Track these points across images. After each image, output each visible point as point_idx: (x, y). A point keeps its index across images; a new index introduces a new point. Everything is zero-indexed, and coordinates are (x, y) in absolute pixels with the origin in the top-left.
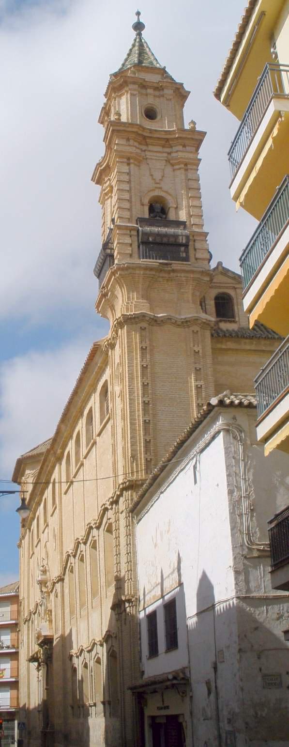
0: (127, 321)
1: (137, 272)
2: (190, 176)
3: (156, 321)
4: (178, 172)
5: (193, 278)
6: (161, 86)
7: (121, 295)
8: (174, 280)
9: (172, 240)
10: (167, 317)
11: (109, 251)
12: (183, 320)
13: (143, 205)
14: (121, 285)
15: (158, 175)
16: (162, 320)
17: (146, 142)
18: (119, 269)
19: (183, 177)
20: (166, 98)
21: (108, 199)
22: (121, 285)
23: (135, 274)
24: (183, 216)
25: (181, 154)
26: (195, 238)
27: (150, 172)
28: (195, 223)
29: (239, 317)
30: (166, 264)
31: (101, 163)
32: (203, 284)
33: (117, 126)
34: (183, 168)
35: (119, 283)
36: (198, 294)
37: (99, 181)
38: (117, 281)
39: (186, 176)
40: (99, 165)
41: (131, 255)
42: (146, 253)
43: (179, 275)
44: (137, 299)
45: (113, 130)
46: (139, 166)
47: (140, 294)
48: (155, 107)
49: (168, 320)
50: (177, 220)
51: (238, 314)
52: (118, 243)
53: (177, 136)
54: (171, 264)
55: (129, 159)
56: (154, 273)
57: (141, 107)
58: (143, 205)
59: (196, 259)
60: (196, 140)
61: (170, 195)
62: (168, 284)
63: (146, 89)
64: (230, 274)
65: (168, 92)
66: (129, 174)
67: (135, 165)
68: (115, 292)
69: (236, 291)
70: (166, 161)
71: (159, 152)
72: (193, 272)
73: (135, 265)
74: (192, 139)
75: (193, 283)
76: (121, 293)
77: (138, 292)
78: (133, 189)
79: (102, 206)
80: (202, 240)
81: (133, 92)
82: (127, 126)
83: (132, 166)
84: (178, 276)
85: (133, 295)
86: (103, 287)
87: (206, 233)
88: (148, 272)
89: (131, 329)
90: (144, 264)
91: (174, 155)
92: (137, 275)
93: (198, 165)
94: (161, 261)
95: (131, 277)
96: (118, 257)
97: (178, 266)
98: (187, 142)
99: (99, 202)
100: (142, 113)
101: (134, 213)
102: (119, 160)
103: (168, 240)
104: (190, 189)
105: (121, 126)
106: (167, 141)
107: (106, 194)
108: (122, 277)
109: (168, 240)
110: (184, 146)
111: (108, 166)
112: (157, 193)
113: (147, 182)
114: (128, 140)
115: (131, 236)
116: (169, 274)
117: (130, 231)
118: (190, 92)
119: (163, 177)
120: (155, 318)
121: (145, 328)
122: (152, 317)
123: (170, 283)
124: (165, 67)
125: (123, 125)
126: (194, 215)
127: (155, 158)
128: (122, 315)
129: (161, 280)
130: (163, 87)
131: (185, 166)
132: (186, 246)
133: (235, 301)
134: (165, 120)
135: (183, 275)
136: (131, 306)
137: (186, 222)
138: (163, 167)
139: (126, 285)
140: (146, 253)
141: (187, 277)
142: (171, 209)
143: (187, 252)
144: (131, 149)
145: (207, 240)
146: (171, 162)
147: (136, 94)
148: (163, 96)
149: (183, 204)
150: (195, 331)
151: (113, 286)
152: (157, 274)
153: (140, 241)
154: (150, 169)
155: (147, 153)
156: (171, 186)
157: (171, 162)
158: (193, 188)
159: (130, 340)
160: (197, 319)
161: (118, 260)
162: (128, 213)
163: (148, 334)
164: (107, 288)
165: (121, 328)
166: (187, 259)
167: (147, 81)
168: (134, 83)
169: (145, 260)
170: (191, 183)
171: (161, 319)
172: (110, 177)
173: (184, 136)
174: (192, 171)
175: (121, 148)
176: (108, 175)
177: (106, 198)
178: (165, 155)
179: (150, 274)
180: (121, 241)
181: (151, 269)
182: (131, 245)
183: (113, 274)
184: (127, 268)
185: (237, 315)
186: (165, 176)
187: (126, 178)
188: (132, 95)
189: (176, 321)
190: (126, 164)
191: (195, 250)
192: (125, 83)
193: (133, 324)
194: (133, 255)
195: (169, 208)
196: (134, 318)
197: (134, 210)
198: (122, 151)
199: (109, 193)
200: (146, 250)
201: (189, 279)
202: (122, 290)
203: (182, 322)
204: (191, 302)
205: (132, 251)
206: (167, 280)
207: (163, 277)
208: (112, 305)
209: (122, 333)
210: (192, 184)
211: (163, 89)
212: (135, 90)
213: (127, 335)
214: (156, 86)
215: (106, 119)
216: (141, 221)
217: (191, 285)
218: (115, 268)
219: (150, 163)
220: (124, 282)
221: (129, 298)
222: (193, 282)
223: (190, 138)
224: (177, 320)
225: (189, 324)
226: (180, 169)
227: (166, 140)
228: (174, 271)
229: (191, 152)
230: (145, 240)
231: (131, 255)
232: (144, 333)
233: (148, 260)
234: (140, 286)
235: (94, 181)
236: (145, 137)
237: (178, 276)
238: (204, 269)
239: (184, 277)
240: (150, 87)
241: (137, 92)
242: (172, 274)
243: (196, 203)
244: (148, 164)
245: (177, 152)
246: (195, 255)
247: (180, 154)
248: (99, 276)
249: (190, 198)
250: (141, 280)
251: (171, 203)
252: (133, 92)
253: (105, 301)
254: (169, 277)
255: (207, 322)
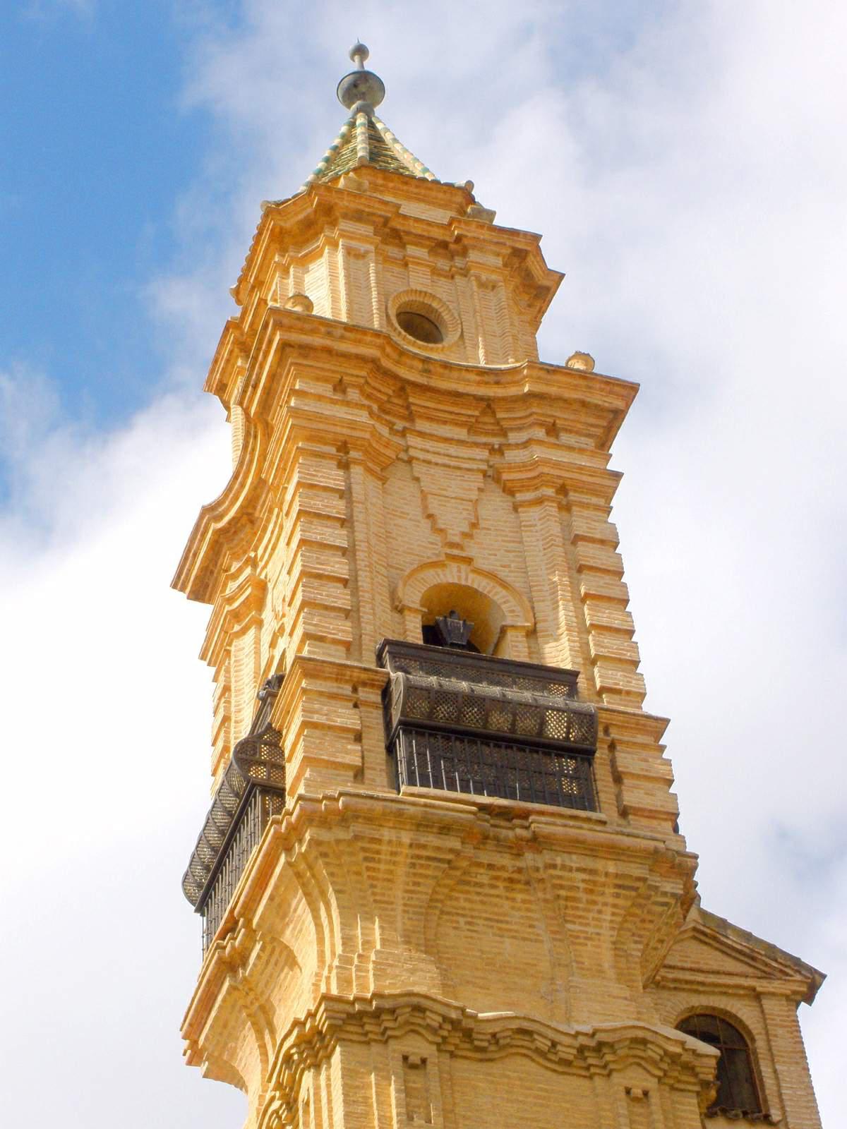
0: (354, 1024)
1: (387, 834)
2: (581, 524)
3: (468, 1034)
4: (531, 515)
5: (617, 876)
6: (458, 239)
7: (313, 935)
8: (541, 880)
9: (527, 725)
10: (515, 1025)
11: (260, 773)
12: (582, 1040)
13: (400, 610)
14: (316, 892)
15: (454, 520)
16: (494, 1035)
17: (408, 407)
18: (309, 818)
19: (556, 529)
20: (478, 278)
21: (244, 631)
22: (316, 892)
23: (379, 841)
24: (559, 654)
25: (533, 452)
26: (615, 734)
27: (425, 507)
28: (609, 683)
29: (783, 1108)
30: (505, 814)
31: (219, 503)
32: (659, 909)
33: (302, 331)
34: (549, 499)
35: (304, 885)
36: (635, 949)
37: (201, 592)
38: (299, 875)
39: (567, 527)
40: (211, 512)
41: (359, 774)
42: (423, 765)
43: (559, 861)
44: (383, 945)
45: (284, 345)
46: (384, 480)
47: (399, 925)
48: (435, 305)
49: (519, 1039)
50: (535, 662)
51: (780, 1095)
52: (305, 724)
53: (526, 389)
54: (525, 815)
55: (344, 447)
56: (454, 843)
57: (384, 297)
58: (400, 610)
59: (624, 812)
60: (598, 410)
61: (504, 584)
62: (513, 900)
63: (403, 246)
64: (732, 940)
65: (487, 261)
66: (345, 494)
67: (369, 471)
68: (283, 932)
69: (761, 1006)
70: (485, 475)
71: (461, 442)
72: (615, 852)
73: (378, 806)
74: (584, 404)
75: (620, 902)
76: (312, 928)
77: (388, 923)
78: (362, 546)
79: (213, 670)
80: (644, 746)
81: (354, 244)
82: (339, 332)
83: (357, 471)
84: (554, 866)
85: (367, 932)
86: (231, 928)
87: (657, 719)
88: (431, 839)
89: (363, 1064)
90: (414, 804)
91: (513, 456)
92: (384, 848)
93: (608, 494)
94: (485, 799)
95: (362, 855)
96: (307, 774)
97: (554, 824)
98: (562, 416)
99: (203, 657)
100: (388, 316)
101: (368, 628)
102: (304, 462)
103: (513, 724)
104: (580, 569)
105: (313, 331)
106: (487, 411)
107: (236, 616)
108: (325, 855)
109: (513, 724)
110: (553, 430)
111: (260, 483)
112: (453, 575)
113: (416, 540)
114: (340, 387)
115: (356, 706)
116: (519, 855)
117: (355, 690)
118: (563, 276)
119: (474, 525)
120: (467, 1023)
121: (424, 1061)
122: (454, 1015)
123: (519, 896)
124: (470, 184)
125: (323, 329)
126: (605, 658)
127: (446, 461)
128: (326, 998)
129: (485, 879)
130: (465, 241)
131: (558, 492)
132: (584, 754)
133: (760, 1044)
134: (476, 346)
135: (575, 861)
136: (359, 969)
137: (575, 674)
138: (474, 495)
139: (337, 892)
140: (423, 765)
141: (592, 872)
142: (510, 635)
143: (585, 780)
144: (353, 416)
145: (662, 748)
146: (505, 476)
147: (367, 252)
148: (465, 272)
149: (557, 618)
150: (637, 1092)
151: (280, 908)
152: (469, 851)
153: (396, 717)
154: (424, 496)
155: (413, 440)
156: (508, 559)
157: (505, 476)
158: (598, 573)
159: (360, 1109)
160: (644, 1042)
161: (307, 786)
162: (347, 626)
163: (435, 1087)
164: (248, 922)
165: (317, 1066)
166: (587, 800)
167: (405, 217)
168: (359, 216)
169: (418, 789)
170: (588, 553)
171: (491, 1029)
172: (256, 550)
173: (553, 390)
174: (586, 513)
175: (310, 406)
176: (249, 543)
177: (237, 628)
178: (484, 454)
179: (438, 849)
180: (315, 718)
181: (445, 829)
182: (358, 738)
183: (284, 843)
184: (345, 818)
185: (773, 1100)
186: (483, 524)
187: (337, 507)
188: (349, 252)
189: (554, 1044)
190: (334, 463)
191: (618, 779)
192: (327, 213)
193: (368, 1043)
194: (368, 774)
195: (503, 630)
196: (377, 1014)
197: (366, 617)
198: (319, 417)
199: (250, 610)
200: (421, 755)
201: (603, 879)
202: (316, 918)
203: (582, 1049)
204: (611, 973)
205: (363, 758)
206: (511, 880)
207: (491, 866)
208: (262, 1008)
209: (317, 1088)
210: (588, 553)
211: (464, 252)
212: (364, 239)
213: (345, 1086)
214: (441, 238)
215: (276, 259)
216: (397, 650)
217: (609, 910)
218: (293, 818)
219: (423, 478)
220: (332, 874)
221: (347, 941)
222: (617, 896)
223: (576, 400)
224: (558, 1038)
225: (608, 1057)
226: (539, 501)
227: (484, 404)
228: (537, 842)
229: (581, 451)
230: (417, 717)
231: (359, 774)
232: (417, 1080)
233: (432, 791)
234: (398, 893)
235: (183, 589)
236: (404, 387)
237: (554, 866)
238: (661, 845)
239: (579, 870)
240: (420, 240)
241: (372, 248)
242: (529, 856)
243: (608, 616)
244: (417, 479)
245: (526, 444)
246: (619, 797)
247: (538, 453)
248: (202, 905)
249: (583, 601)
250: (401, 871)
251: (508, 610)
252: (354, 244)
253: (233, 988)
254: (520, 870)
255: (686, 1057)
